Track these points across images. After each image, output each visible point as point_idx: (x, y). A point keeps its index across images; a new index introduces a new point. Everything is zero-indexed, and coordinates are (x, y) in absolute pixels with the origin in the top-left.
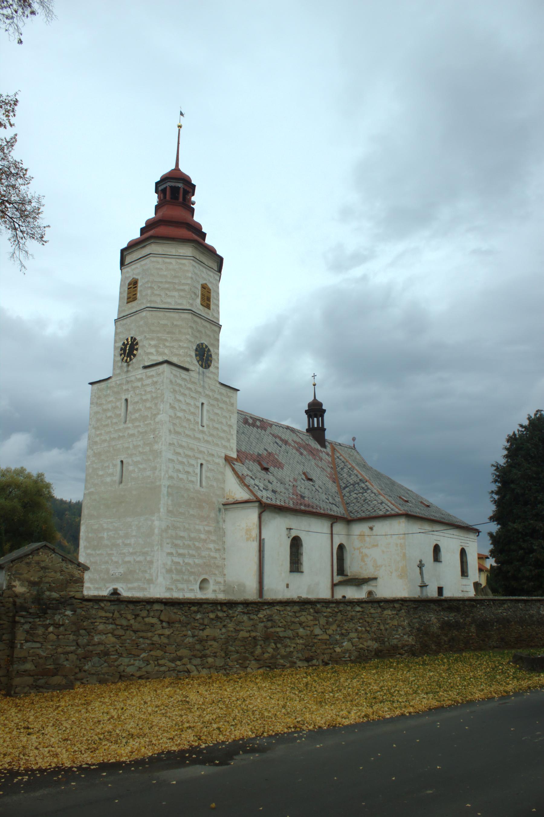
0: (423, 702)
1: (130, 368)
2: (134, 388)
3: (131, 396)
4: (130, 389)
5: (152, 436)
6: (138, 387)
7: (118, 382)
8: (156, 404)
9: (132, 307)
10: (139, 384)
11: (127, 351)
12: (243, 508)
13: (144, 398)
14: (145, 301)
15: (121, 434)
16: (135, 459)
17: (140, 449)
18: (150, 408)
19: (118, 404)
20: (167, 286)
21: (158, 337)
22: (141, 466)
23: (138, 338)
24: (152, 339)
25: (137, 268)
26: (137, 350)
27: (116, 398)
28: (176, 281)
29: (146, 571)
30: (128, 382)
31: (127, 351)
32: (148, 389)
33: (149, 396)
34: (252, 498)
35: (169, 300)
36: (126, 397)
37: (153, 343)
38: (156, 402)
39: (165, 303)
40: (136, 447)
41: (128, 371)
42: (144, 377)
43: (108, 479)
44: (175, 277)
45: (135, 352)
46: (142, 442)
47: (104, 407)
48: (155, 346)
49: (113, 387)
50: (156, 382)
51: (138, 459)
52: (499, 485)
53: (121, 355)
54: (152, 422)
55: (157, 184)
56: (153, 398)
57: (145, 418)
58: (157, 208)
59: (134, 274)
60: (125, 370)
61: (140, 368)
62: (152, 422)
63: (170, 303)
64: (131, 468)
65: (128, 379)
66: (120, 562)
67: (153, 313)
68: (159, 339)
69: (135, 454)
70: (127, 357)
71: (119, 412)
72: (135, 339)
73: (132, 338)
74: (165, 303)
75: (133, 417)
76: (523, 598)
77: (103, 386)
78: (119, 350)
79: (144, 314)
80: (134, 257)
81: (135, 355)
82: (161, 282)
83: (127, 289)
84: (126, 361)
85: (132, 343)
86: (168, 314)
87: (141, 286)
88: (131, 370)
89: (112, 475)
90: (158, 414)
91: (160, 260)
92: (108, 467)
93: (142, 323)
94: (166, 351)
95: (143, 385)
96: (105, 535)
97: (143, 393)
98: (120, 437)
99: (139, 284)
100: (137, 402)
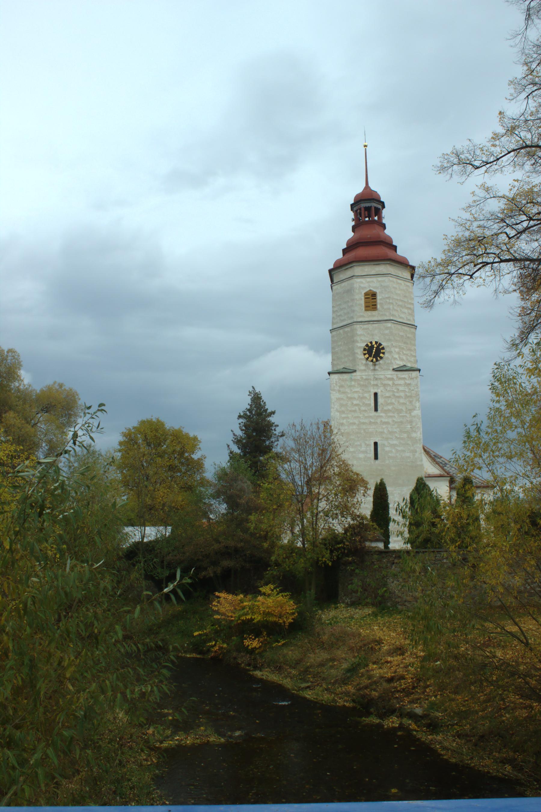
0: (313, 591)
1: (377, 367)
2: (385, 385)
3: (381, 391)
4: (379, 385)
5: (409, 426)
6: (389, 385)
7: (364, 377)
8: (411, 402)
9: (373, 316)
10: (390, 383)
11: (373, 353)
12: (436, 481)
14: (387, 314)
15: (373, 421)
16: (391, 442)
17: (397, 435)
18: (404, 404)
19: (366, 395)
20: (400, 303)
21: (399, 346)
22: (399, 449)
23: (384, 344)
24: (396, 347)
25: (373, 282)
26: (384, 353)
27: (363, 390)
28: (406, 300)
31: (373, 353)
32: (401, 388)
33: (402, 394)
34: (442, 473)
35: (403, 316)
36: (376, 391)
37: (397, 350)
38: (411, 400)
39: (401, 318)
40: (391, 433)
42: (395, 378)
43: (361, 456)
44: (405, 296)
46: (398, 429)
47: (349, 395)
48: (398, 353)
49: (358, 380)
50: (410, 384)
51: (395, 442)
53: (365, 354)
54: (408, 415)
55: (352, 206)
56: (406, 397)
57: (399, 411)
58: (354, 229)
59: (370, 286)
61: (389, 369)
62: (408, 415)
64: (387, 449)
65: (376, 376)
67: (395, 325)
69: (392, 438)
70: (373, 357)
71: (369, 402)
72: (380, 344)
73: (376, 343)
74: (401, 318)
77: (345, 377)
78: (362, 350)
79: (389, 325)
80: (366, 270)
82: (397, 300)
83: (363, 298)
84: (372, 361)
85: (378, 348)
87: (381, 299)
88: (379, 369)
89: (365, 452)
90: (414, 410)
91: (395, 280)
92: (361, 445)
93: (387, 332)
94: (404, 358)
95: (393, 384)
97: (396, 391)
98: (371, 423)
99: (379, 297)
100: (389, 397)
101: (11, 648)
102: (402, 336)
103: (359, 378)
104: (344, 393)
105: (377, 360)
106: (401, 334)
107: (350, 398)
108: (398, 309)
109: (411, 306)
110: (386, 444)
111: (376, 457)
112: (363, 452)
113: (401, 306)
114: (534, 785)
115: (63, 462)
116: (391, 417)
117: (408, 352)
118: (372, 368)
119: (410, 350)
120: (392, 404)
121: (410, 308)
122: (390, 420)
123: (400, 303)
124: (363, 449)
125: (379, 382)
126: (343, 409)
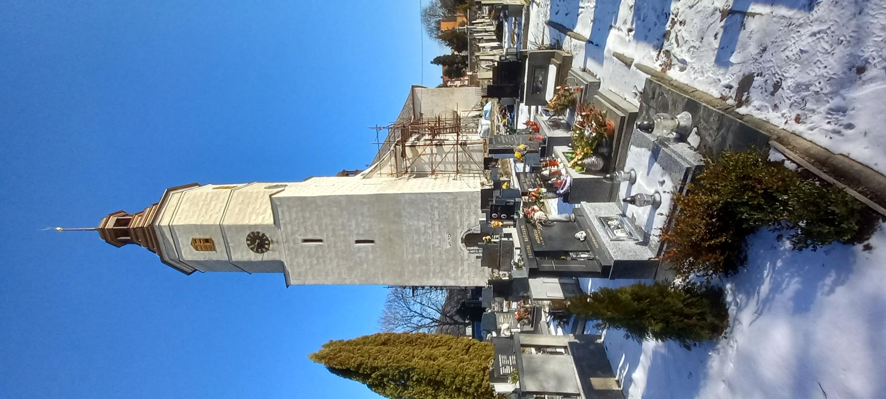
1: (274, 240)
13: (301, 220)
16: (354, 226)
19: (306, 250)
20: (204, 210)
26: (258, 233)
29: (447, 206)
30: (287, 241)
33: (300, 214)
35: (218, 208)
36: (300, 241)
41: (277, 242)
45: (260, 235)
48: (258, 215)
52: (796, 279)
60: (276, 245)
63: (221, 207)
66: (439, 237)
68: (251, 214)
75: (318, 232)
76: (525, 81)
81: (263, 235)
86: (230, 208)
89: (367, 252)
95: (290, 223)
96: (417, 256)
100: (305, 228)
101: (517, 244)
102: (240, 210)
103: (289, 259)
104: (306, 272)
105: (267, 239)
106: (237, 210)
107: (311, 266)
108: (209, 214)
109: (210, 196)
110: (356, 232)
111: (372, 242)
112: (367, 256)
113: (207, 210)
114: (644, 119)
115: (512, 160)
116: (326, 226)
117: (259, 202)
118: (276, 245)
119: (257, 198)
120: (312, 225)
121: (212, 198)
122: (330, 228)
123: (204, 210)
124: (363, 255)
125: (291, 239)
126: (323, 274)
